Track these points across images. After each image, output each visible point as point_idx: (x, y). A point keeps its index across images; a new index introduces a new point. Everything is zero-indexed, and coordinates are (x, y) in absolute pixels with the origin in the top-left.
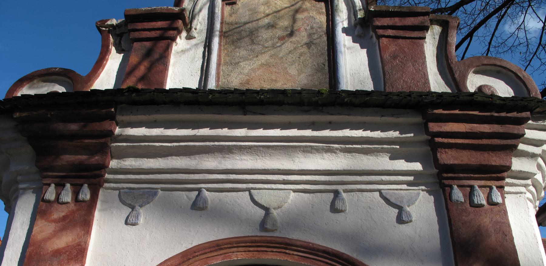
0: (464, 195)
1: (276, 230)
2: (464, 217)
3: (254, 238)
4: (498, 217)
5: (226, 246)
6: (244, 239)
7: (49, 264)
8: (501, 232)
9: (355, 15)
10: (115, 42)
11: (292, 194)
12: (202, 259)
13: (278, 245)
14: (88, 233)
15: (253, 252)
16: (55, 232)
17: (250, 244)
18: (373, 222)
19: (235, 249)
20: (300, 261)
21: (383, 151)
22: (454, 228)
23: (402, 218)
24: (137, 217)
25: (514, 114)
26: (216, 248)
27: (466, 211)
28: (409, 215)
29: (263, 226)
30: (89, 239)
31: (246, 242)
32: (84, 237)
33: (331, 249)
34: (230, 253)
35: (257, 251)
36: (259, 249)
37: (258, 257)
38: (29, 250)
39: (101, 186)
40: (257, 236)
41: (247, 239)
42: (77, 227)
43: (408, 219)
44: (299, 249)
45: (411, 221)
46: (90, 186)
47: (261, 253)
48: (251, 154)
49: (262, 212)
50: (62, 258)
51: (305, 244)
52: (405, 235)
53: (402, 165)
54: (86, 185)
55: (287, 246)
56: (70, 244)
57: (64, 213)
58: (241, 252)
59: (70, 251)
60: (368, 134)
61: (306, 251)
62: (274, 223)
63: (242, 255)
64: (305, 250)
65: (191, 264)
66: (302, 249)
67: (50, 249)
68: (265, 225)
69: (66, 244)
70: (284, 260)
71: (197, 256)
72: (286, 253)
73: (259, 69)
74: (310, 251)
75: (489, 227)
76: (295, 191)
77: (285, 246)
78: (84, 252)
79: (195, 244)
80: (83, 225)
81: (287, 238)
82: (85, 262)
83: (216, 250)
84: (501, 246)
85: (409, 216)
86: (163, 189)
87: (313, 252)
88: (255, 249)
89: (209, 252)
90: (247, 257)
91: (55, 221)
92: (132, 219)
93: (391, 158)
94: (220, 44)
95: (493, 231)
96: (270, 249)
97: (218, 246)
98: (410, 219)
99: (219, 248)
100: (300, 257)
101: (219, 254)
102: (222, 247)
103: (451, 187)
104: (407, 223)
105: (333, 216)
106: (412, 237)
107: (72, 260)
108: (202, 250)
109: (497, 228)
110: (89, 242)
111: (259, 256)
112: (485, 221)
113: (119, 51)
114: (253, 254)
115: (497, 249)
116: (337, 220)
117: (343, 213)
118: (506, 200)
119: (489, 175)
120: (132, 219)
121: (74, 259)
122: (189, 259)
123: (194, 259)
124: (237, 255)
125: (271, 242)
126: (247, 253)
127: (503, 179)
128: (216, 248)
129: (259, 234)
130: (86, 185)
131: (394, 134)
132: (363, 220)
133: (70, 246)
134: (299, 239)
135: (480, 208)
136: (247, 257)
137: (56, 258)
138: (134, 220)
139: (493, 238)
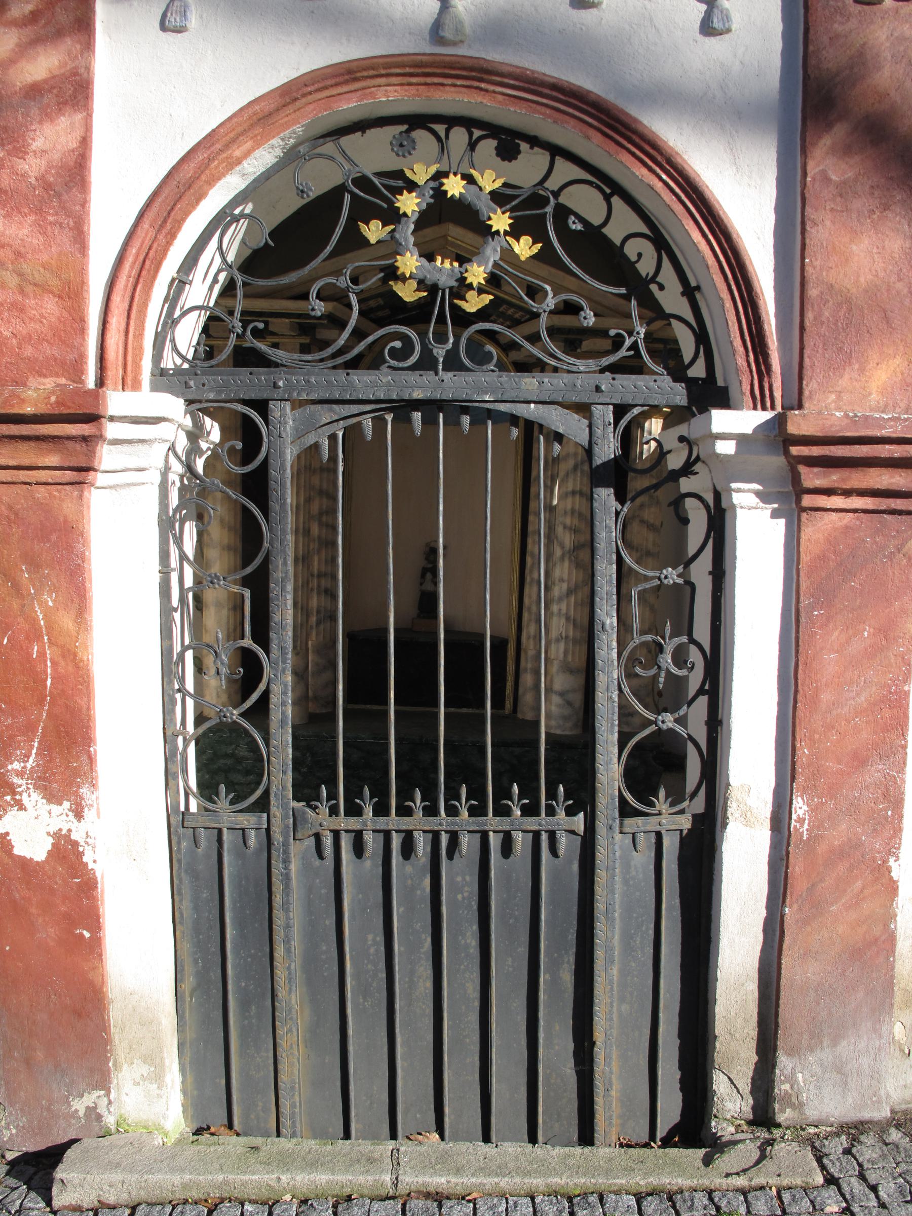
1: (462, 42)
2: (836, 26)
3: (419, 58)
4: (905, 29)
5: (365, 74)
6: (400, 59)
7: (23, 114)
8: (904, 60)
12: (320, 100)
13: (464, 73)
14: (89, 48)
15: (417, 87)
16: (20, 46)
17: (412, 70)
18: (654, 29)
19: (383, 81)
20: (507, 105)
22: (811, 48)
23: (712, 22)
24: (184, 14)
26: (346, 77)
27: (843, 12)
28: (727, 17)
29: (437, 33)
30: (93, 60)
31: (403, 66)
32: (82, 58)
33: (567, 82)
34: (374, 87)
36: (429, 80)
37: (427, 96)
40: (424, 54)
41: (405, 59)
42: (64, 35)
43: (724, 24)
44: (506, 81)
45: (729, 31)
47: (432, 89)
49: (434, 4)
50: (45, 101)
51: (518, 71)
52: (714, 60)
55: (483, 75)
56: (56, 72)
57: (32, 6)
58: (395, 85)
59: (60, 88)
61: (520, 86)
62: (459, 26)
63: (396, 91)
64: (517, 83)
65: (298, 109)
66: (512, 82)
67: (18, 84)
68: (440, 31)
69: (48, 72)
70: (476, 103)
71: (310, 93)
72: (481, 89)
74: (526, 85)
75: (883, 48)
77: (479, 75)
78: (88, 88)
79: (304, 69)
80: (76, 31)
81: (484, 59)
82: (92, 109)
83: (346, 82)
84: (899, 88)
85: (727, 18)
87: (532, 87)
89: (332, 86)
90: (406, 95)
92: (175, 19)
95: (889, 58)
96: (449, 81)
97: (350, 72)
98: (727, 26)
99: (353, 76)
100: (507, 98)
101: (353, 89)
102: (359, 75)
104: (721, 34)
106: (726, 64)
107: (66, 104)
108: (319, 81)
109: (899, 51)
110: (94, 67)
111: (429, 94)
112: (877, 35)
114: (418, 90)
115: (889, 95)
116: (583, 24)
117: (595, 9)
119: (340, 530)
120: (175, 19)
121: (70, 103)
122: (296, 99)
123: (304, 100)
124: (386, 91)
125: (451, 66)
126: (406, 88)
128: (346, 77)
129: (429, 49)
132: (634, 26)
133: (57, 76)
134: (506, 61)
135: (874, 7)
136: (406, 95)
137: (35, 101)
138: (178, 19)
139: (886, 72)
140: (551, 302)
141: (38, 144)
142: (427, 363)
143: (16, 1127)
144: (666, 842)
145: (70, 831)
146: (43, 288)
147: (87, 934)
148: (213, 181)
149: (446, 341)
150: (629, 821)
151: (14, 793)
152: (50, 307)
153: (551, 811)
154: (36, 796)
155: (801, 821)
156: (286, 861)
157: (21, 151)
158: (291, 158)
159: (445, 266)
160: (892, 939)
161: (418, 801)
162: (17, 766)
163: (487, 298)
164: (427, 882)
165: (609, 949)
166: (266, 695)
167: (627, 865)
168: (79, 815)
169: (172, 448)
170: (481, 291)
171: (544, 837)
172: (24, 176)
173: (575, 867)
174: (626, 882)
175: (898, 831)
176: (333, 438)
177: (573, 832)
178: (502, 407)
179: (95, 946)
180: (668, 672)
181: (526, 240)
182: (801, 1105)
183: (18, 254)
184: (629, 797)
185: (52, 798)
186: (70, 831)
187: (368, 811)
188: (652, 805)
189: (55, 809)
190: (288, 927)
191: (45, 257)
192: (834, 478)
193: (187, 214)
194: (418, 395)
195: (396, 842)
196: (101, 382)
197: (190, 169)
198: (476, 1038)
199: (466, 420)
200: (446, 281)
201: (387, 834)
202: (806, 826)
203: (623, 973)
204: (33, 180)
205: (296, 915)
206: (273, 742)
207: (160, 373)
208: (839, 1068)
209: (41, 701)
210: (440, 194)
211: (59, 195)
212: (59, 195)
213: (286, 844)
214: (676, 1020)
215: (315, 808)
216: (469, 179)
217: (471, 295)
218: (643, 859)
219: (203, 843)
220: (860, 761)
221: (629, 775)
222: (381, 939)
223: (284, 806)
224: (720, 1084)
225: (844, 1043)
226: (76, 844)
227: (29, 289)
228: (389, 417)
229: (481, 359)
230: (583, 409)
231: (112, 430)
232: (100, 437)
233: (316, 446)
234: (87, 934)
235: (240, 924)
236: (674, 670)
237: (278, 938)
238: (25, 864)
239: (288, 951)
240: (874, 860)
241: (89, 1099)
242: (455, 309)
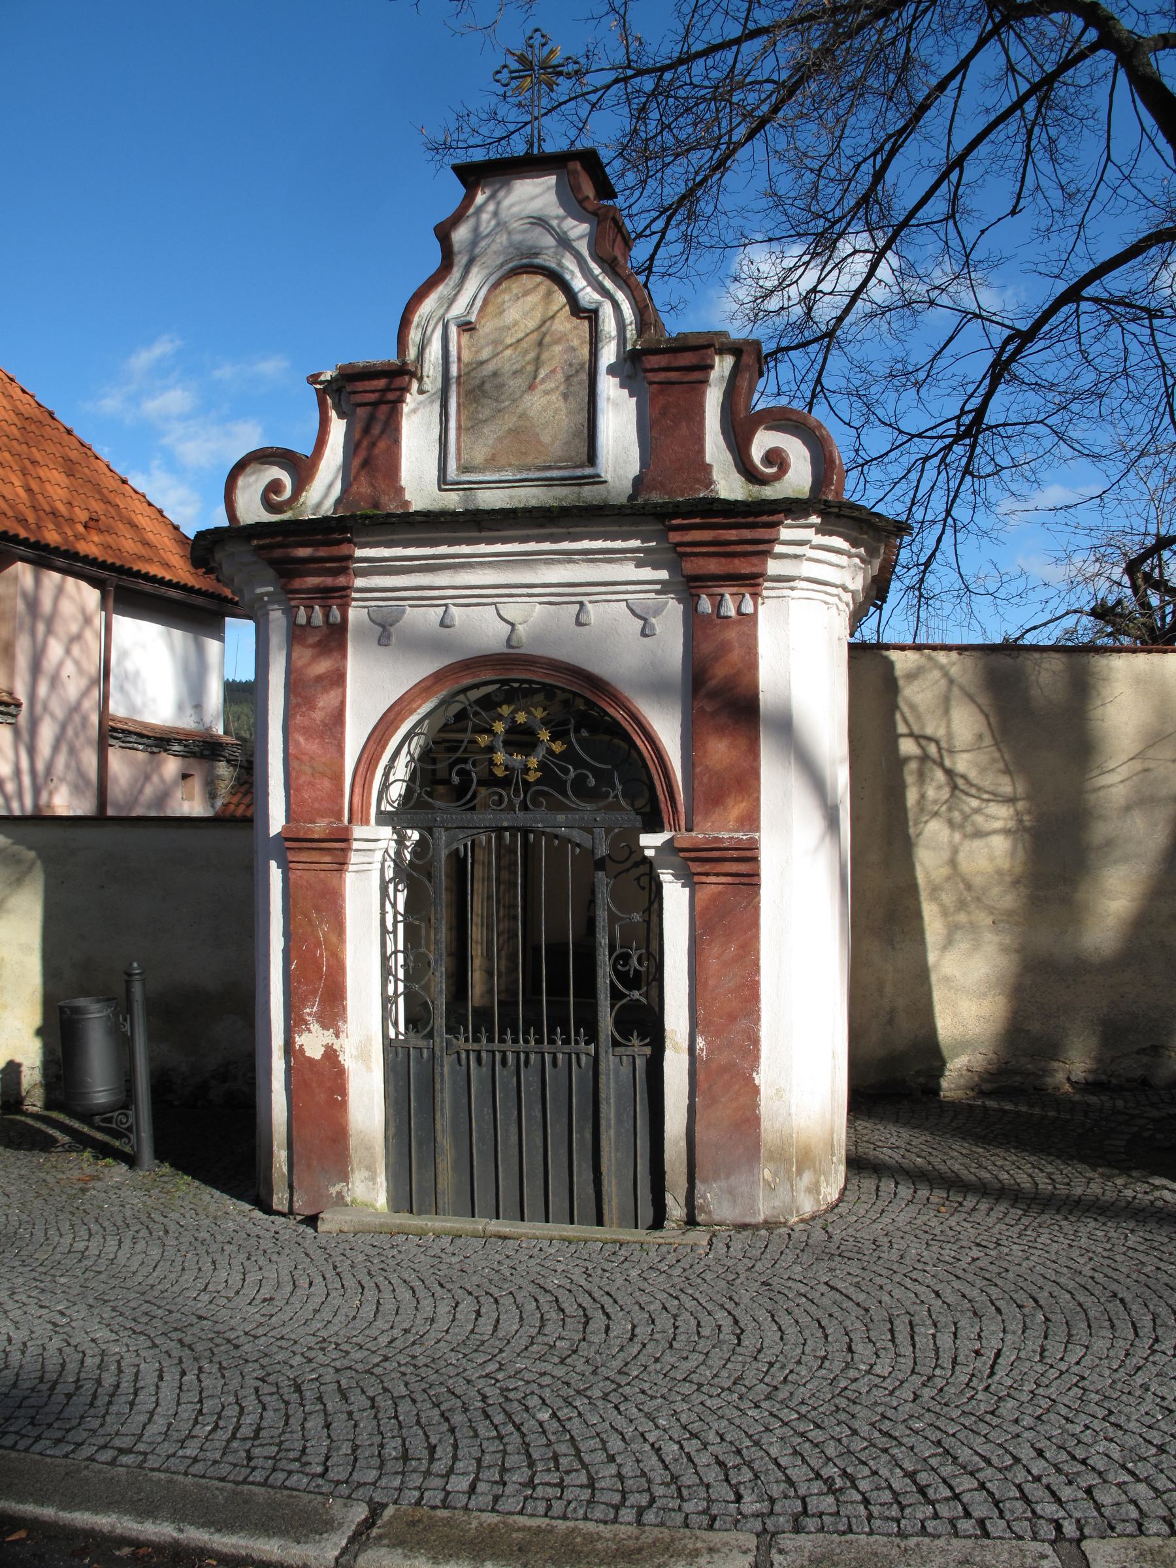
0: (713, 605)
9: (625, 347)
10: (333, 402)
11: (538, 606)
21: (627, 559)
25: (765, 519)
28: (653, 628)
38: (293, 676)
39: (349, 605)
46: (339, 606)
48: (493, 568)
53: (647, 573)
60: (609, 544)
73: (505, 437)
76: (541, 603)
86: (411, 606)
91: (310, 646)
93: (637, 566)
94: (459, 405)
103: (699, 596)
105: (581, 628)
113: (341, 415)
118: (760, 608)
127: (759, 585)
131: (635, 543)
140: (572, 774)
141: (321, 704)
142: (511, 807)
144: (638, 1062)
146: (323, 775)
148: (402, 721)
149: (519, 796)
150: (617, 1049)
151: (306, 1024)
152: (327, 784)
153: (577, 1043)
155: (702, 1050)
156: (442, 1066)
157: (313, 708)
158: (442, 703)
159: (518, 757)
160: (757, 1119)
162: (308, 1010)
164: (515, 1080)
165: (608, 1120)
167: (617, 1073)
168: (337, 1036)
169: (386, 851)
170: (536, 770)
171: (574, 1056)
172: (314, 720)
173: (591, 1073)
174: (617, 1083)
175: (757, 1058)
176: (466, 846)
177: (587, 1054)
178: (548, 830)
179: (343, 1105)
180: (635, 969)
182: (710, 1212)
183: (312, 758)
184: (616, 1034)
185: (325, 1027)
187: (484, 1040)
188: (630, 1041)
189: (325, 1032)
190: (442, 1102)
191: (324, 760)
192: (707, 867)
193: (391, 737)
194: (505, 824)
195: (498, 1057)
196: (350, 821)
197: (391, 716)
198: (541, 1169)
199: (532, 836)
200: (517, 765)
201: (493, 1052)
203: (618, 1134)
205: (447, 1095)
207: (379, 812)
208: (731, 1192)
209: (321, 978)
210: (514, 721)
212: (330, 729)
213: (442, 1057)
214: (648, 1164)
215: (458, 1039)
216: (529, 712)
217: (531, 773)
218: (626, 1069)
219: (400, 1056)
220: (732, 1018)
221: (617, 1023)
222: (491, 1111)
223: (442, 1037)
224: (669, 1199)
225: (733, 1178)
226: (335, 1051)
227: (317, 775)
228: (493, 835)
229: (537, 805)
230: (589, 831)
231: (356, 845)
232: (349, 849)
233: (457, 850)
235: (418, 1100)
236: (638, 967)
237: (438, 1108)
238: (311, 1060)
239: (442, 1115)
241: (338, 1188)
242: (525, 782)
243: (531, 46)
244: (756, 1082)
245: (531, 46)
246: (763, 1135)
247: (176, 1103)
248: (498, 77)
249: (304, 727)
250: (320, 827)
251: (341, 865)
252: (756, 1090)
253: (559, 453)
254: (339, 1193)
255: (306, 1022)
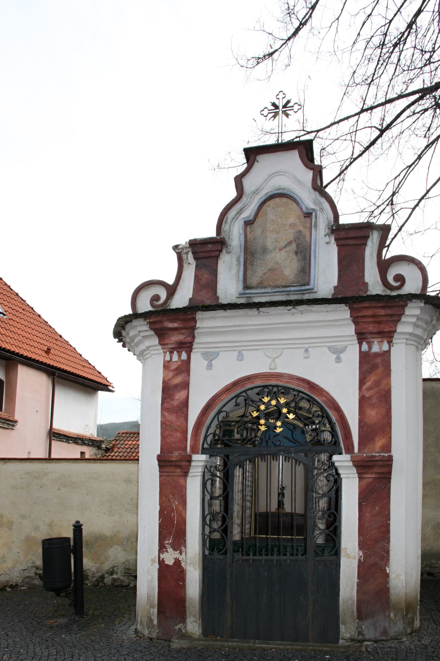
35: (267, 380)
46: (186, 352)
54: (184, 352)
88: (266, 379)
118: (392, 348)
130: (184, 352)
141: (177, 398)
143: (161, 633)
145: (179, 558)
146: (177, 430)
147: (181, 583)
152: (179, 435)
153: (297, 555)
154: (171, 549)
157: (173, 400)
160: (388, 590)
161: (264, 552)
162: (167, 542)
163: (281, 429)
166: (227, 526)
168: (181, 554)
170: (280, 427)
175: (388, 560)
181: (291, 414)
185: (175, 550)
186: (179, 558)
187: (251, 554)
189: (176, 552)
202: (362, 558)
204: (175, 406)
206: (228, 537)
207: (203, 448)
211: (181, 409)
217: (278, 428)
226: (180, 561)
234: (181, 583)
240: (382, 568)
241: (179, 626)
243: (278, 99)
244: (388, 571)
245: (278, 99)
246: (391, 597)
247: (89, 584)
248: (262, 113)
249: (168, 409)
250: (175, 455)
251: (186, 474)
252: (388, 576)
253: (293, 279)
254: (180, 629)
255: (165, 548)
